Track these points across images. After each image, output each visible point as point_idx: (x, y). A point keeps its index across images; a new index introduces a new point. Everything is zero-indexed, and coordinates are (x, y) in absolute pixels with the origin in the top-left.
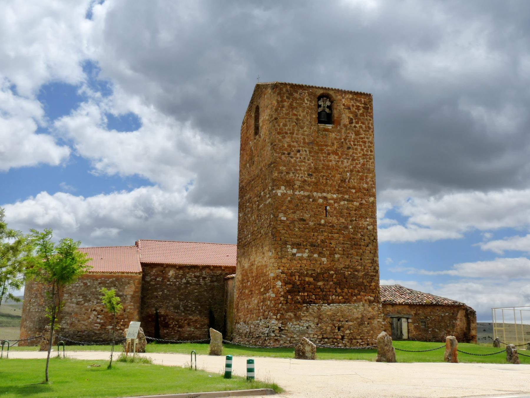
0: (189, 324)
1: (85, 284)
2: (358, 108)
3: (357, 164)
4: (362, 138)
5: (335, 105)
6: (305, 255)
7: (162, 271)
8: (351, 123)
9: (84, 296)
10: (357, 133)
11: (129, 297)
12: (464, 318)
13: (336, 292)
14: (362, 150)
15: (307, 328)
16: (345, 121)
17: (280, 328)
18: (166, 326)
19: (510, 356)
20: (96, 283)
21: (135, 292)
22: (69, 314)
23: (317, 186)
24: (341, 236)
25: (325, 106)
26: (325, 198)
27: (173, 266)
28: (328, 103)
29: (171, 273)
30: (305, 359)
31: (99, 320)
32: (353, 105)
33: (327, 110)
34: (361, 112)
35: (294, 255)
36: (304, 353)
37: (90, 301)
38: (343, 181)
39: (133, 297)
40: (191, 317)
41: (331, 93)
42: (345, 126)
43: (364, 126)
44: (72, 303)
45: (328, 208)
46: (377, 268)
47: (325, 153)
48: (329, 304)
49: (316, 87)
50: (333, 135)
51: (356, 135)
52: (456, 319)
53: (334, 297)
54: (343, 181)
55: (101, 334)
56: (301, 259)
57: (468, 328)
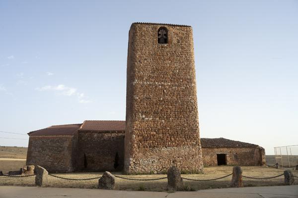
0: (105, 161)
1: (43, 142)
2: (183, 34)
3: (183, 65)
4: (186, 50)
5: (169, 33)
6: (151, 119)
7: (90, 135)
8: (178, 42)
9: (43, 148)
10: (182, 48)
11: (66, 148)
12: (258, 153)
13: (171, 140)
14: (186, 57)
15: (152, 162)
16: (175, 41)
17: (134, 162)
18: (93, 162)
19: (288, 179)
20: (49, 141)
21: (69, 145)
22: (35, 157)
23: (157, 79)
24: (174, 107)
25: (163, 34)
26: (162, 85)
27: (96, 132)
28: (165, 33)
29: (95, 135)
30: (106, 189)
31: (50, 160)
32: (180, 33)
33: (165, 37)
34: (184, 36)
35: (143, 119)
36: (105, 184)
37: (45, 150)
38: (174, 74)
39: (68, 148)
40: (106, 157)
41: (166, 26)
42: (174, 44)
43: (187, 44)
44: (36, 151)
45: (165, 91)
46: (198, 125)
47: (162, 60)
48: (166, 147)
49: (156, 24)
50: (168, 50)
51: (182, 49)
52: (253, 154)
53: (170, 143)
54: (174, 74)
55: (51, 167)
56: (147, 121)
57: (261, 159)
